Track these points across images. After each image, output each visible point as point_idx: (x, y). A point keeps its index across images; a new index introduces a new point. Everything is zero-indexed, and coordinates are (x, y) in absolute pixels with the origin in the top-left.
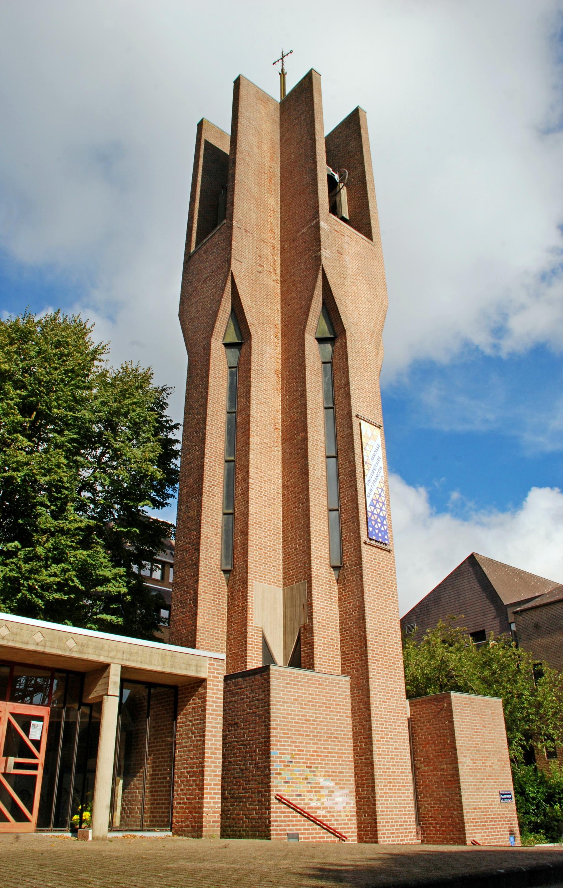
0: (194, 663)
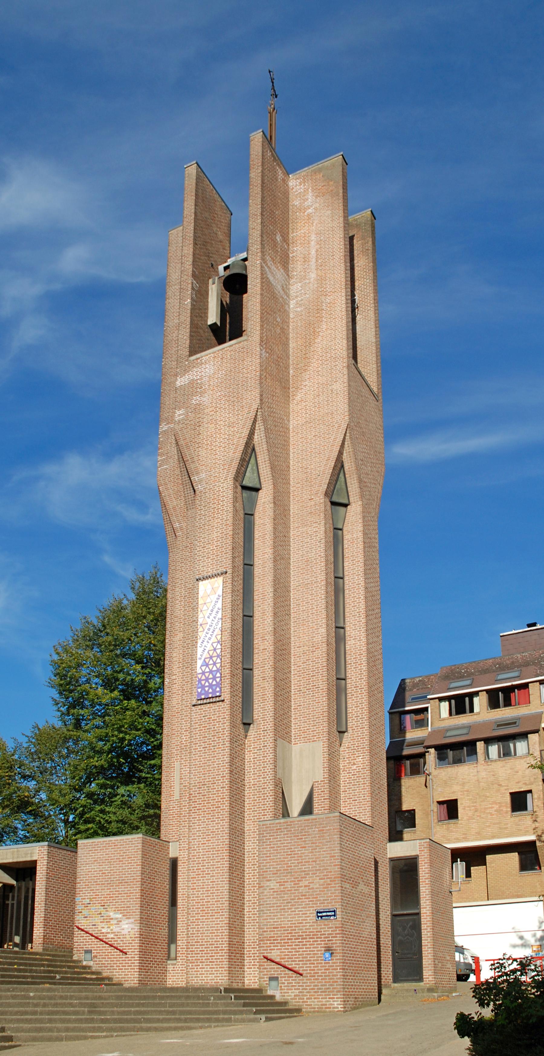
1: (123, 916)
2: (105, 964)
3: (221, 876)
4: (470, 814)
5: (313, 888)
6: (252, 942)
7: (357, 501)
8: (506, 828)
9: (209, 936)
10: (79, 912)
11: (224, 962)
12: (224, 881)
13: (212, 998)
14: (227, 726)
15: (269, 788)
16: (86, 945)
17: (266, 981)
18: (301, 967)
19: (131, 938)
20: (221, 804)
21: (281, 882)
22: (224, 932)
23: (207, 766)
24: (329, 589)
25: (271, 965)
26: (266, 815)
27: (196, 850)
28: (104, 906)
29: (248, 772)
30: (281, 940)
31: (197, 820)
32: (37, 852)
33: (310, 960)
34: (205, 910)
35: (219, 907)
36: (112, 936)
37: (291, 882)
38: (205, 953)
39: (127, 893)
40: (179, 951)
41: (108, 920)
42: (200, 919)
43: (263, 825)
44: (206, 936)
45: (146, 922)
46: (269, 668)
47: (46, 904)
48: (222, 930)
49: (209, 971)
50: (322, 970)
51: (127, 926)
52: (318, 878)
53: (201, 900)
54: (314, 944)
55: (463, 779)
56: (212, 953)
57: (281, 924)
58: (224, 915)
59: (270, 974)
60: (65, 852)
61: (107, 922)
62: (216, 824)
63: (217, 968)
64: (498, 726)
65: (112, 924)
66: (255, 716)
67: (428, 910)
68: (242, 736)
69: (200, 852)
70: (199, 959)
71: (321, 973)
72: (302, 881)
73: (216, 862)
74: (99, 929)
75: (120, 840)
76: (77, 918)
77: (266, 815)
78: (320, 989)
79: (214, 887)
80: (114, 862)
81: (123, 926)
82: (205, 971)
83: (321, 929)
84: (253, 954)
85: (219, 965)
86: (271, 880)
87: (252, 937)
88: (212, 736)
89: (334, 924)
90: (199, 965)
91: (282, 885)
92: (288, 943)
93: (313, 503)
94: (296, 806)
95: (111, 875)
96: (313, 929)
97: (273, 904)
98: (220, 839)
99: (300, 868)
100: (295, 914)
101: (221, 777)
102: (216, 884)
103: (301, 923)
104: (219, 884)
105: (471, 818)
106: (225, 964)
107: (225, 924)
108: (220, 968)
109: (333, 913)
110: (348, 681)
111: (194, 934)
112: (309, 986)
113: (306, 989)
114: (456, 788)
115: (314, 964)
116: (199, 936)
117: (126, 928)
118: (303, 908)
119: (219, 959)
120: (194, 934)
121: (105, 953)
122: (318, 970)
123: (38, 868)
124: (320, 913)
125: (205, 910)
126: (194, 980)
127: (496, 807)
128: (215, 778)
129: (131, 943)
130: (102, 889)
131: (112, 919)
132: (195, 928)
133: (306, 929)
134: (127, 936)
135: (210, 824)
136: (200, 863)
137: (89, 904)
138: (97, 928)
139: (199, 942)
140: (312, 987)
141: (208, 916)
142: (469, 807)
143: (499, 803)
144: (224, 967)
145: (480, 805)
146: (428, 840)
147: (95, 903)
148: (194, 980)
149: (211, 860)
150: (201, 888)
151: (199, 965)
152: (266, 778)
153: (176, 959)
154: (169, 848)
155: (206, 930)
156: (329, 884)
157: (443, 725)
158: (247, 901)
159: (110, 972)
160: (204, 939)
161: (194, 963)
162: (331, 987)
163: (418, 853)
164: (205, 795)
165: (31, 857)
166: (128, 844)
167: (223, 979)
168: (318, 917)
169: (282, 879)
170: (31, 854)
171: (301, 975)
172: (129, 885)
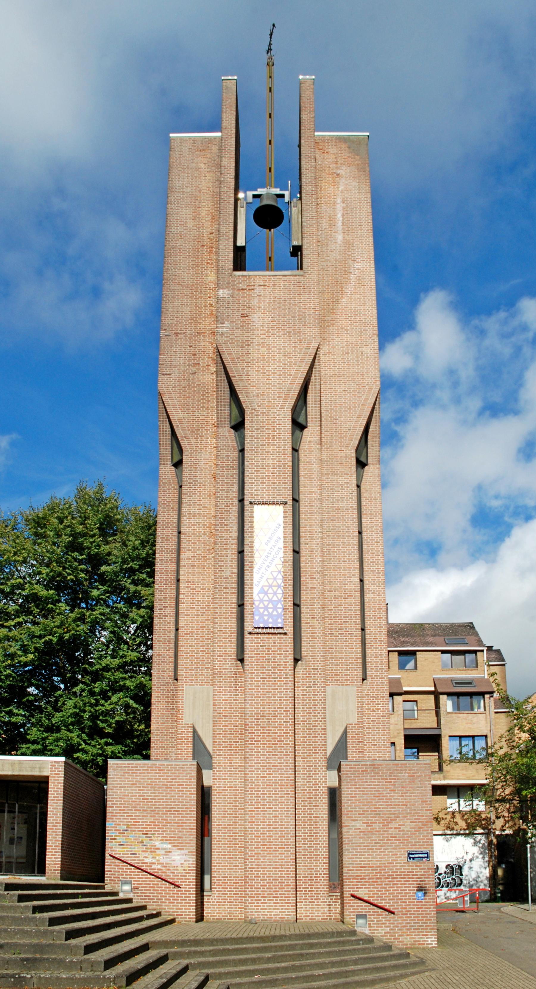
0: (38, 766)
5: (403, 831)
19: (184, 870)
21: (368, 823)
26: (318, 753)
27: (254, 783)
36: (159, 867)
41: (154, 850)
51: (178, 857)
52: (409, 821)
59: (358, 912)
65: (159, 855)
72: (392, 823)
74: (141, 858)
77: (318, 753)
78: (413, 926)
83: (412, 869)
86: (357, 820)
87: (303, 871)
89: (426, 866)
91: (369, 826)
97: (360, 843)
99: (390, 811)
100: (384, 855)
103: (391, 863)
109: (426, 855)
118: (393, 849)
124: (412, 854)
131: (158, 849)
133: (396, 869)
134: (179, 868)
137: (126, 830)
138: (139, 857)
140: (404, 925)
156: (421, 828)
162: (425, 925)
166: (178, 770)
168: (410, 858)
169: (369, 820)
171: (393, 913)
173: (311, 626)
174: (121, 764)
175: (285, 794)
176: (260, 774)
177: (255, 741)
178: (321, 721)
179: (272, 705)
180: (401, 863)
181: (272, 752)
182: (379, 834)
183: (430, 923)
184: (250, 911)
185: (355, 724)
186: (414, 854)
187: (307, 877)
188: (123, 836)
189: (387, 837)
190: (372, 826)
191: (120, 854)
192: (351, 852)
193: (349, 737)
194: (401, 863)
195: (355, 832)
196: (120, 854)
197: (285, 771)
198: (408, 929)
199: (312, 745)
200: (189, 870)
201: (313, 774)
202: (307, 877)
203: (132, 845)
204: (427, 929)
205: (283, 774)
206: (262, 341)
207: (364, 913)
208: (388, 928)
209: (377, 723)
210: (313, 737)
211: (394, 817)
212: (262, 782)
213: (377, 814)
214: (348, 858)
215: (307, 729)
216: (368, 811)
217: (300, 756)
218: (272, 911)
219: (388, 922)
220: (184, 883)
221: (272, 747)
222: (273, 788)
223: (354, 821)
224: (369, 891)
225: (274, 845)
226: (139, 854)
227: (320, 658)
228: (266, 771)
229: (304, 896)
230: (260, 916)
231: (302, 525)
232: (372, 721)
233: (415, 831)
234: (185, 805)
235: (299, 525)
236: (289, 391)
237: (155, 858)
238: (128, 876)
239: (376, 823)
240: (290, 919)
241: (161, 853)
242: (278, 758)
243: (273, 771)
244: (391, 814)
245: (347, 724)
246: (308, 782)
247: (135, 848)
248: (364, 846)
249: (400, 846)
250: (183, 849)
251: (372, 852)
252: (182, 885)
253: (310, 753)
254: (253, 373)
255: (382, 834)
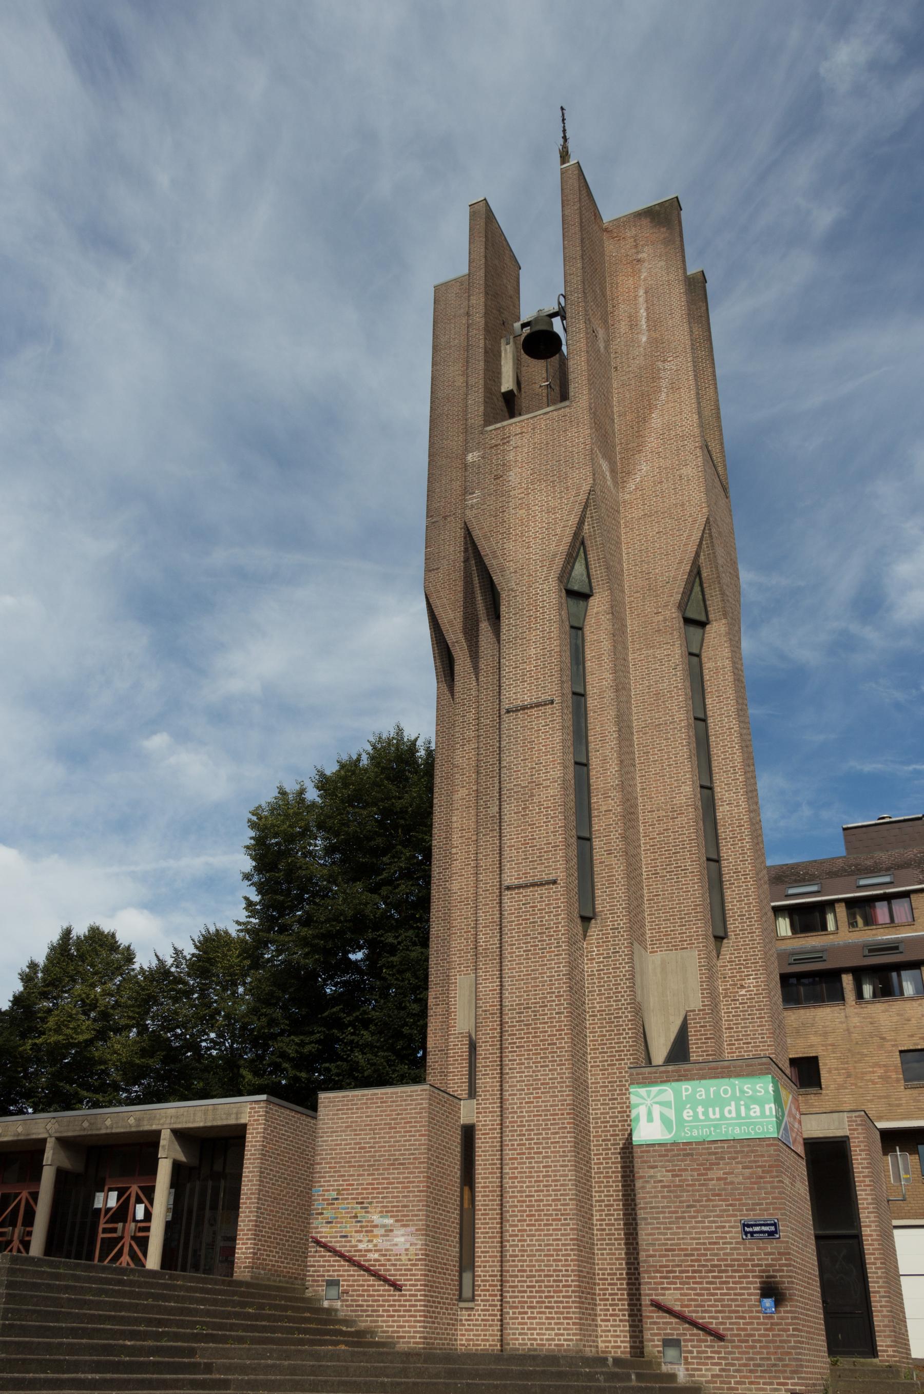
1: (397, 1221)
2: (362, 1306)
3: (560, 1156)
4: (840, 1080)
5: (732, 1183)
6: (609, 1274)
7: (720, 619)
8: (899, 1105)
9: (543, 1261)
10: (317, 1214)
11: (570, 1307)
12: (567, 1166)
13: (602, 1378)
14: (563, 919)
15: (626, 1017)
16: (329, 1271)
17: (657, 1346)
18: (722, 1323)
19: (410, 1260)
20: (557, 1039)
21: (675, 1170)
22: (569, 1255)
23: (532, 979)
24: (691, 734)
25: (665, 1318)
26: (623, 1060)
27: (516, 1112)
28: (362, 1203)
29: (589, 992)
30: (681, 1272)
31: (518, 1064)
32: (248, 1111)
33: (738, 1312)
34: (534, 1215)
35: (560, 1210)
36: (376, 1256)
37: (692, 1170)
38: (537, 1292)
39: (404, 1183)
40: (479, 1286)
41: (369, 1229)
42: (526, 1230)
43: (638, 1074)
44: (537, 1261)
45: (432, 1232)
46: (617, 838)
47: (259, 1199)
48: (566, 1250)
49: (544, 1324)
50: (760, 1330)
51: (402, 1239)
52: (740, 1166)
53: (527, 1196)
54: (742, 1283)
55: (824, 1027)
56: (549, 1292)
57: (679, 1244)
58: (568, 1224)
59: (665, 1334)
60: (288, 1112)
61: (366, 1231)
62: (550, 1070)
63: (559, 1318)
64: (870, 951)
65: (376, 1236)
66: (599, 908)
67: (875, 1231)
68: (580, 937)
69: (524, 1117)
70: (526, 1302)
71: (760, 1335)
72: (713, 1169)
73: (553, 1133)
74: (354, 1243)
75: (392, 1093)
76: (315, 1223)
77: (623, 1060)
78: (759, 1365)
79: (550, 1176)
80: (380, 1129)
81: (396, 1240)
82: (537, 1324)
83: (752, 1255)
84: (610, 1294)
85: (562, 1313)
86: (656, 1167)
87: (608, 1264)
88: (539, 933)
89: (775, 1248)
90: (526, 1313)
91: (677, 1176)
92: (695, 1277)
93: (661, 618)
94: (660, 1050)
95: (375, 1152)
96: (738, 1254)
97: (663, 1207)
98: (557, 1096)
99: (708, 1148)
100: (703, 1228)
101: (556, 997)
102: (552, 1171)
103: (715, 1243)
104: (559, 1171)
105: (840, 1087)
106: (574, 1313)
107: (572, 1239)
108: (565, 1318)
109: (773, 1228)
110: (724, 863)
111: (517, 1256)
112: (737, 1359)
113: (734, 1365)
114: (814, 1039)
115: (744, 1318)
116: (525, 1261)
117: (399, 1242)
118: (717, 1216)
119: (562, 1302)
120: (517, 1256)
121: (363, 1286)
122: (752, 1329)
123: (249, 1137)
124: (749, 1226)
125: (534, 1215)
126: (517, 1339)
127: (880, 1071)
128: (546, 998)
129: (411, 1270)
130: (358, 1175)
131: (376, 1226)
132: (517, 1246)
133: (724, 1254)
134: (403, 1257)
135: (539, 1071)
136: (524, 1135)
137: (337, 1199)
138: (350, 1241)
139: (525, 1271)
140: (744, 1361)
141: (540, 1225)
142: (837, 1069)
143: (885, 1066)
144: (571, 1318)
145: (855, 1068)
146: (863, 1113)
147: (347, 1199)
148: (517, 1339)
149: (543, 1129)
150: (527, 1177)
151: (526, 1313)
152: (620, 1000)
153: (473, 1300)
154: (460, 1109)
155: (537, 1250)
156: (761, 1177)
157: (783, 947)
158: (597, 1201)
159: (371, 1321)
160: (534, 1266)
161: (517, 1308)
162: (780, 1363)
163: (848, 1133)
164: (530, 1025)
165: (237, 1119)
166: (405, 1100)
167: (571, 1340)
168: (746, 1233)
169: (677, 1165)
170: (237, 1114)
171: (720, 1337)
172: (407, 1168)
173: (606, 866)
174: (334, 1098)
175: (559, 1128)
176: (524, 1099)
177: (517, 1047)
178: (626, 1009)
179: (540, 990)
180: (731, 1243)
181: (540, 1062)
182: (693, 1191)
183: (789, 1359)
184: (511, 1332)
185: (699, 1010)
186: (752, 1226)
187: (615, 1274)
188: (332, 1209)
189: (706, 1196)
190: (681, 1175)
191: (327, 1237)
192: (650, 1224)
193: (691, 1031)
194: (731, 1243)
195: (655, 1187)
196: (327, 1237)
197: (559, 1092)
198: (751, 1371)
199: (614, 1047)
200: (416, 1260)
201: (618, 1095)
202: (615, 1274)
203: (342, 1223)
204: (785, 1371)
205: (557, 1096)
206: (520, 502)
207: (675, 1337)
208: (718, 1368)
209: (749, 1007)
210: (615, 1035)
211: (716, 1159)
212: (527, 1112)
213: (688, 1155)
214: (646, 1235)
215: (607, 1023)
216: (673, 1150)
217: (598, 1066)
218: (544, 1330)
219: (716, 1356)
220: (408, 1283)
221: (540, 1054)
222: (543, 1120)
223: (652, 1167)
224: (681, 1295)
225: (545, 1215)
226: (351, 1237)
227: (621, 912)
228: (532, 1094)
229: (611, 1308)
230: (526, 1342)
231: (590, 726)
232: (740, 1004)
233: (752, 1183)
234: (413, 1154)
235: (586, 727)
236: (555, 555)
237: (372, 1241)
238: (336, 1273)
239: (687, 1170)
240: (571, 1347)
241: (379, 1233)
242: (550, 1070)
243: (542, 1093)
244: (710, 1154)
245: (687, 1012)
246: (610, 1108)
247: (346, 1227)
248: (669, 1213)
249: (729, 1210)
250: (407, 1226)
251: (683, 1223)
252: (406, 1285)
253: (612, 1060)
254: (510, 545)
255: (698, 1191)
